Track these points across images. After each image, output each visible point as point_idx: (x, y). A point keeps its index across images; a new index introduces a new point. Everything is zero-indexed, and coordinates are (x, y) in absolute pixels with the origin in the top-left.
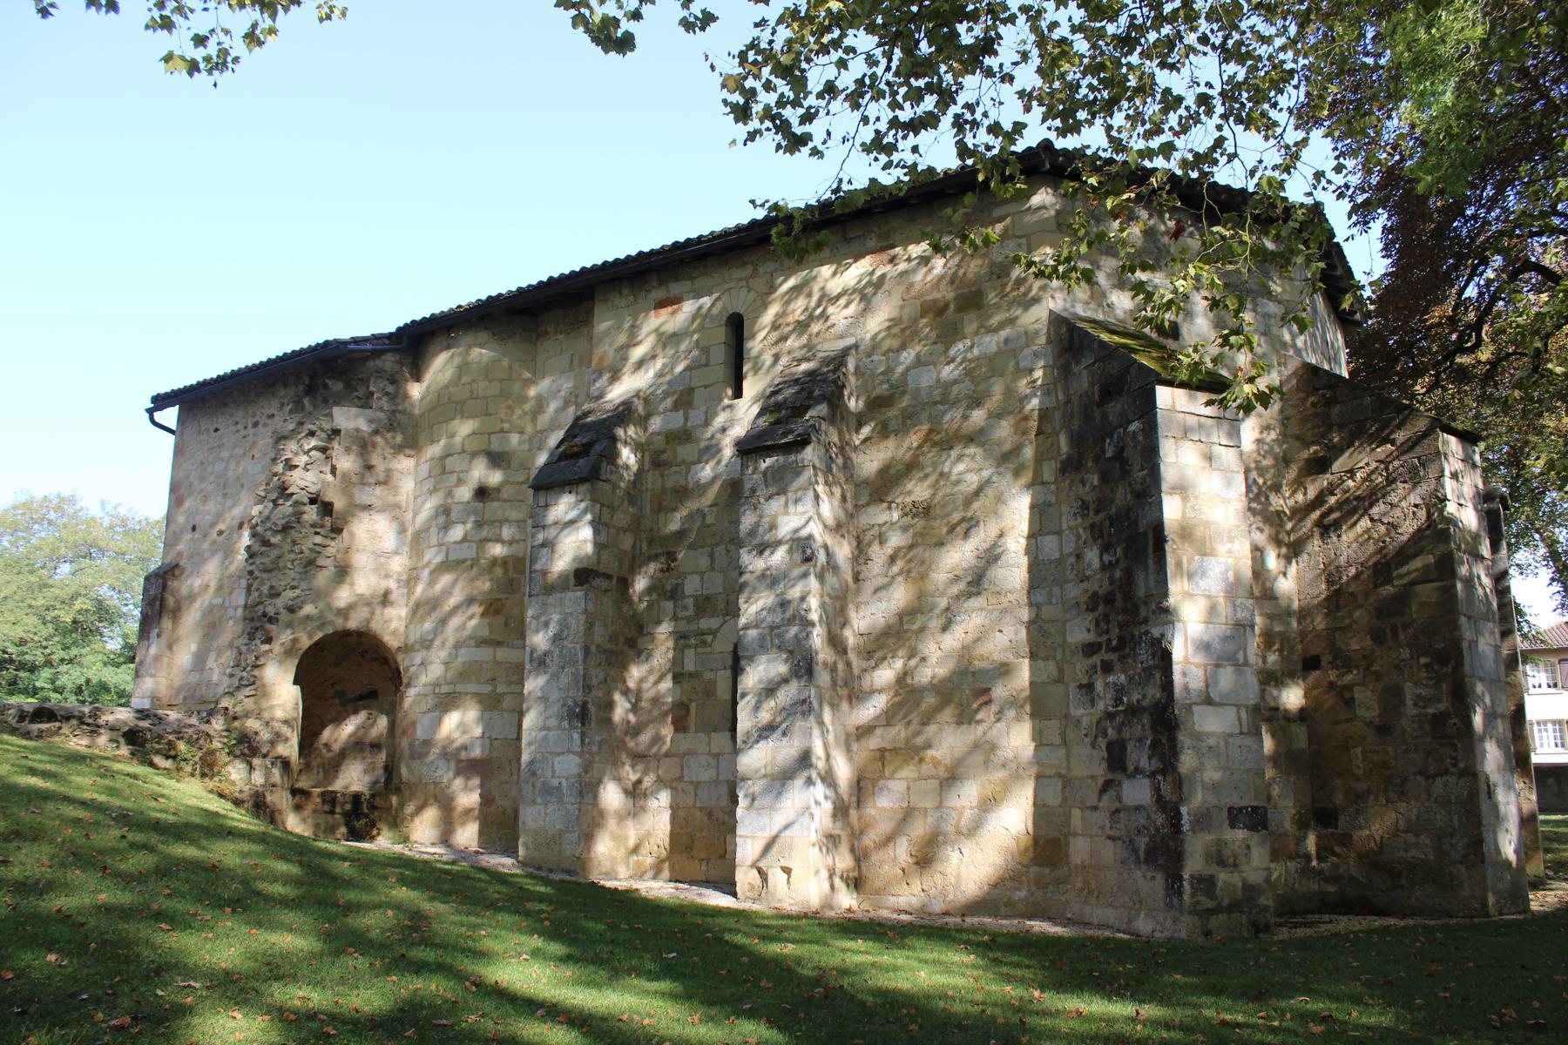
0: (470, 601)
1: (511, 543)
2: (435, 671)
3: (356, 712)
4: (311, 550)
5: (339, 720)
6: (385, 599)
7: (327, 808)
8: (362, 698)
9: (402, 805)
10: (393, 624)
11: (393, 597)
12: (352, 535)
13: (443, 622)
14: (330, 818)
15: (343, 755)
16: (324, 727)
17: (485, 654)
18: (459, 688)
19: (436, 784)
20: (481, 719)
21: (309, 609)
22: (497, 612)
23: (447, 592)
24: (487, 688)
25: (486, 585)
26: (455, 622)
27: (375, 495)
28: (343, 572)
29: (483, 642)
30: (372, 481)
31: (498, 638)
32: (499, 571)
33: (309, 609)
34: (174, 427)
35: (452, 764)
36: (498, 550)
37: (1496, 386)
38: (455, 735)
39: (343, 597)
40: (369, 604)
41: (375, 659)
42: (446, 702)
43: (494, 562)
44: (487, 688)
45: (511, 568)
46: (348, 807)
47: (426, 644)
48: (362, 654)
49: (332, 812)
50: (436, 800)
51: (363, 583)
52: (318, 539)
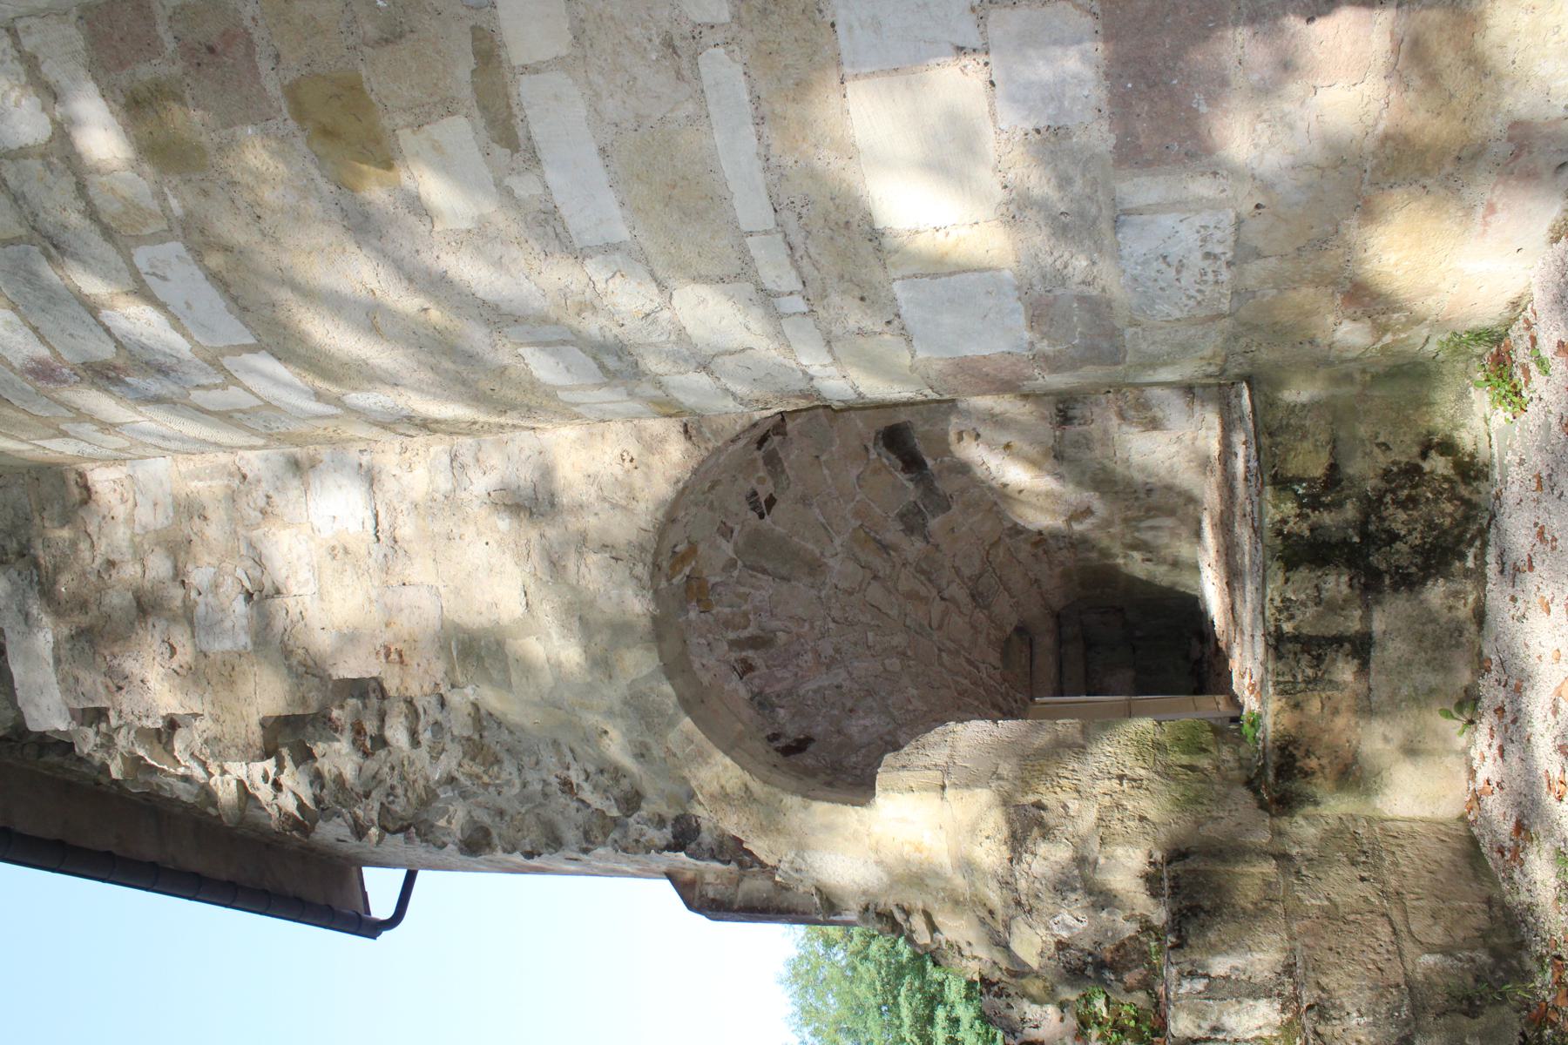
0: (363, 226)
1: (51, 94)
2: (709, 313)
3: (964, 468)
4: (436, 754)
5: (997, 499)
6: (531, 503)
7: (1345, 672)
8: (912, 463)
9: (1327, 363)
10: (613, 463)
11: (525, 476)
12: (351, 638)
13: (498, 316)
14: (1393, 650)
15: (1106, 482)
16: (1017, 531)
17: (557, 113)
18: (752, 210)
19: (1244, 253)
20: (900, 63)
21: (616, 747)
22: (351, 94)
23: (371, 318)
24: (722, 71)
25: (259, 158)
26: (471, 272)
27: (214, 575)
28: (475, 650)
29: (505, 132)
30: (178, 593)
31: (464, 67)
32: (189, 120)
33: (616, 747)
34: (401, 874)
35: (1142, 190)
36: (103, 140)
37: (1346, 618)
38: (989, 181)
39: (554, 648)
40: (555, 565)
41: (772, 461)
42: (840, 248)
43: (161, 152)
44: (722, 71)
45: (145, 72)
46: (1337, 584)
47: (616, 363)
48: (763, 506)
49: (1361, 648)
50: (1321, 244)
51: (493, 580)
52: (397, 734)
